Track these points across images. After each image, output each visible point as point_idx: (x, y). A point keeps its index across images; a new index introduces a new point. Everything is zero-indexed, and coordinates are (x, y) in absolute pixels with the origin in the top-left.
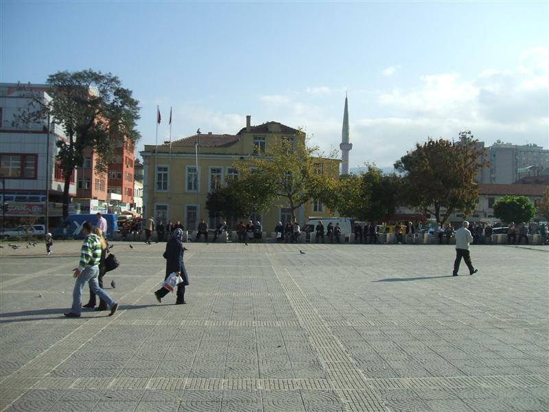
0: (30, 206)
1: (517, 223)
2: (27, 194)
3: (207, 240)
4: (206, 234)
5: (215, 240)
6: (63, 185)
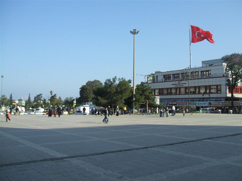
0: (219, 103)
1: (107, 111)
2: (218, 98)
3: (236, 113)
4: (236, 111)
5: (238, 113)
6: (231, 94)
